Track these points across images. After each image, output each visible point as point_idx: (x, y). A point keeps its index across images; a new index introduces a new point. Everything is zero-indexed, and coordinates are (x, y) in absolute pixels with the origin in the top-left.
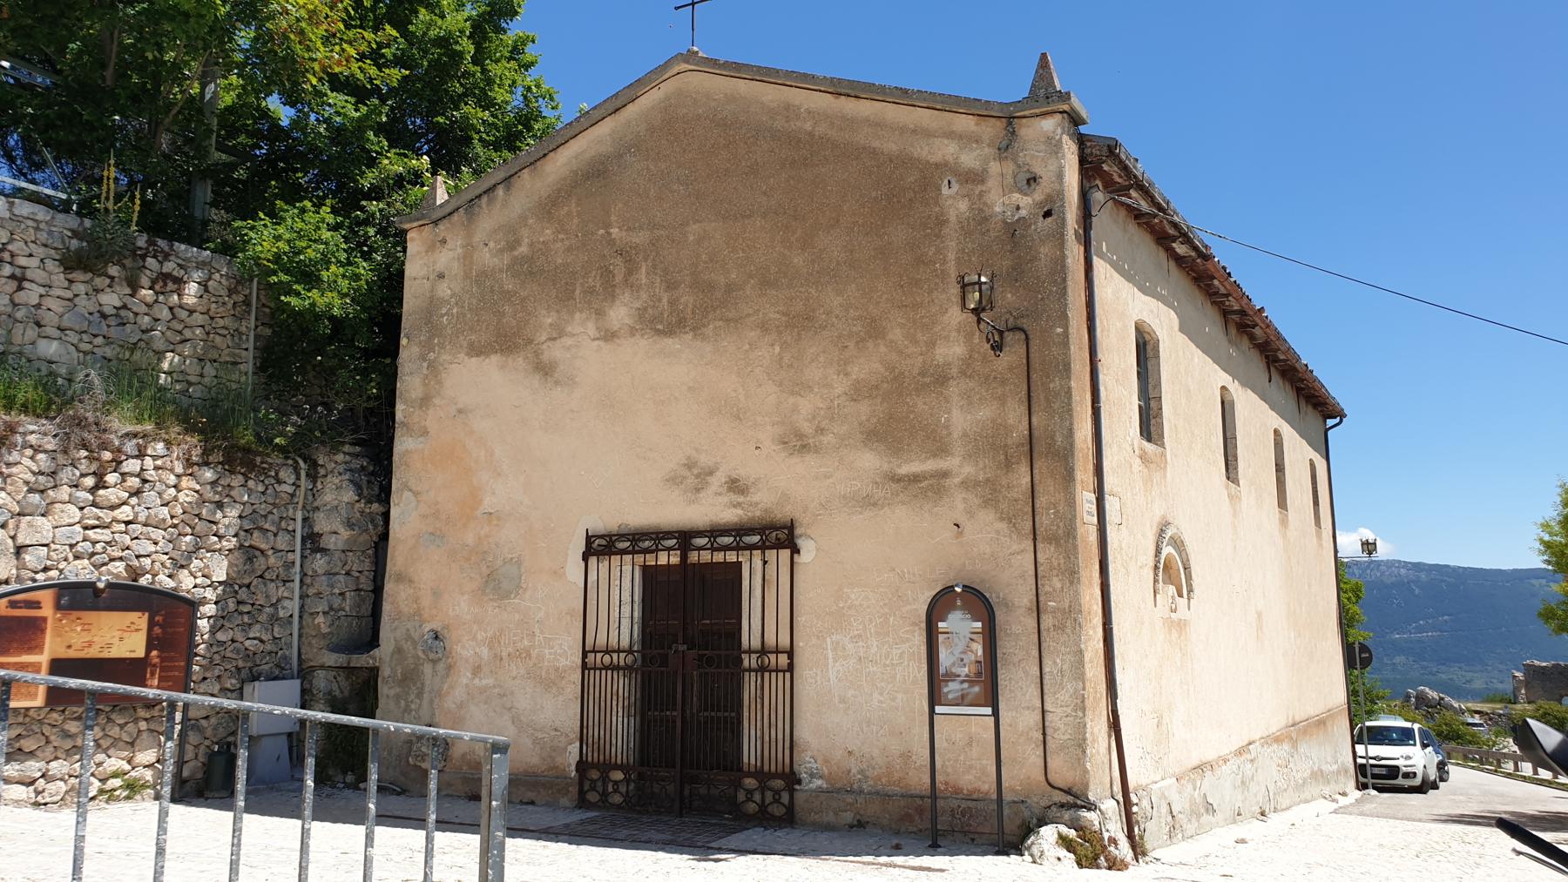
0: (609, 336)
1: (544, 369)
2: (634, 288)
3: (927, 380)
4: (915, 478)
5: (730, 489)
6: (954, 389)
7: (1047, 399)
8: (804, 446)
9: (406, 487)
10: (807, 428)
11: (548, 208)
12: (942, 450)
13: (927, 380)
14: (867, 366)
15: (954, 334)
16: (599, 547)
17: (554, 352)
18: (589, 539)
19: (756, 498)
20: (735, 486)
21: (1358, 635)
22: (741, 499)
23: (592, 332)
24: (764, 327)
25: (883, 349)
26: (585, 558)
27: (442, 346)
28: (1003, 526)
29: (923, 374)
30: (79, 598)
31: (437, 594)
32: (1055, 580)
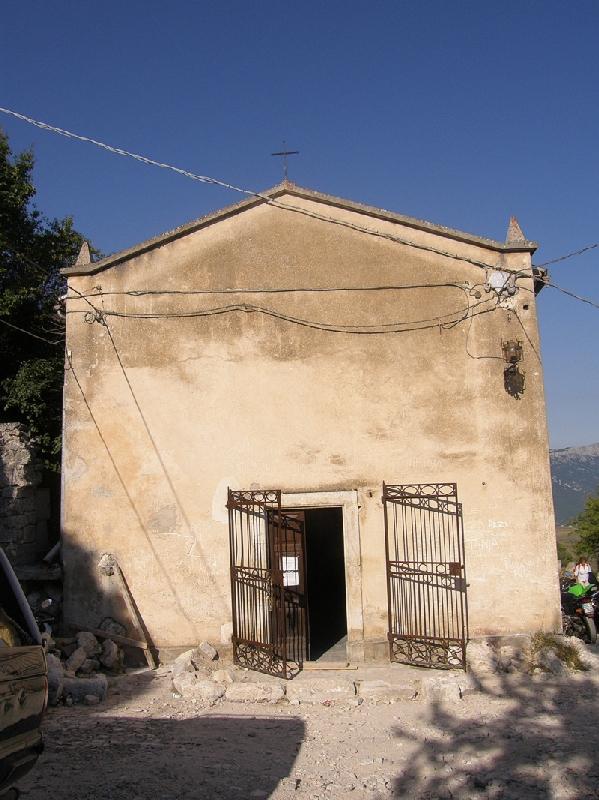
0: (239, 359)
1: (184, 378)
2: (257, 329)
3: (461, 397)
4: (456, 456)
5: (333, 462)
6: (478, 403)
7: (532, 412)
8: (383, 436)
9: (507, 401)
10: (385, 425)
11: (188, 269)
12: (471, 438)
13: (461, 397)
14: (422, 387)
15: (476, 371)
16: (237, 502)
17: (192, 368)
18: (230, 494)
19: (352, 468)
20: (337, 460)
21: (562, 543)
22: (341, 468)
23: (226, 356)
24: (351, 359)
25: (431, 377)
26: (384, 503)
27: (101, 359)
28: (511, 483)
29: (458, 393)
30: (298, 673)
31: (108, 529)
32: (540, 513)
